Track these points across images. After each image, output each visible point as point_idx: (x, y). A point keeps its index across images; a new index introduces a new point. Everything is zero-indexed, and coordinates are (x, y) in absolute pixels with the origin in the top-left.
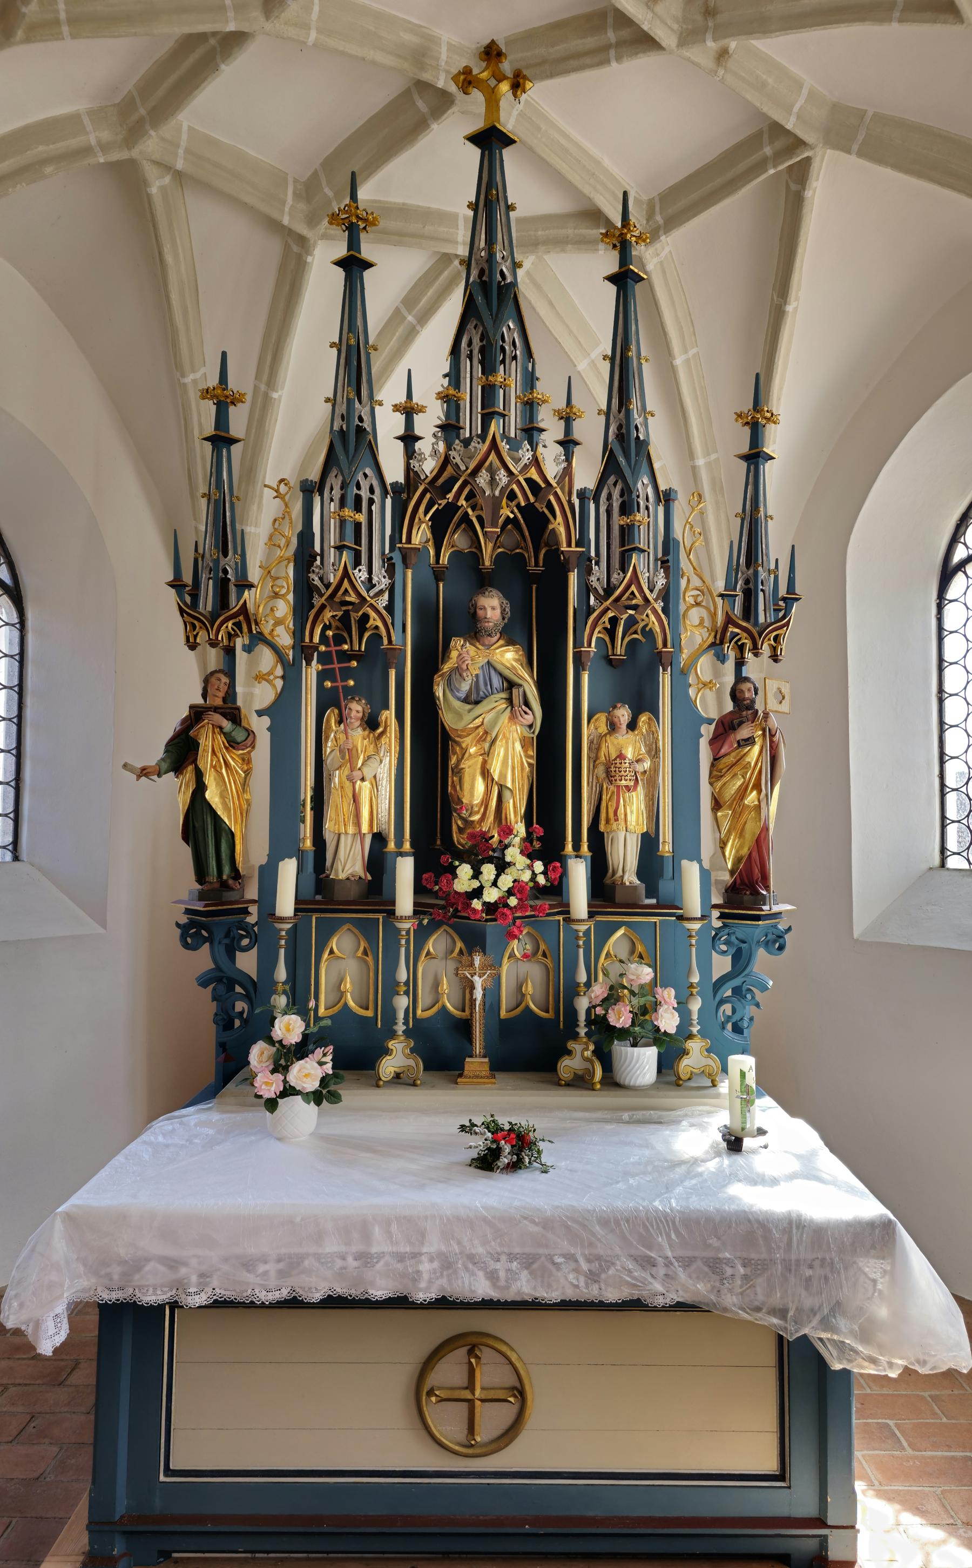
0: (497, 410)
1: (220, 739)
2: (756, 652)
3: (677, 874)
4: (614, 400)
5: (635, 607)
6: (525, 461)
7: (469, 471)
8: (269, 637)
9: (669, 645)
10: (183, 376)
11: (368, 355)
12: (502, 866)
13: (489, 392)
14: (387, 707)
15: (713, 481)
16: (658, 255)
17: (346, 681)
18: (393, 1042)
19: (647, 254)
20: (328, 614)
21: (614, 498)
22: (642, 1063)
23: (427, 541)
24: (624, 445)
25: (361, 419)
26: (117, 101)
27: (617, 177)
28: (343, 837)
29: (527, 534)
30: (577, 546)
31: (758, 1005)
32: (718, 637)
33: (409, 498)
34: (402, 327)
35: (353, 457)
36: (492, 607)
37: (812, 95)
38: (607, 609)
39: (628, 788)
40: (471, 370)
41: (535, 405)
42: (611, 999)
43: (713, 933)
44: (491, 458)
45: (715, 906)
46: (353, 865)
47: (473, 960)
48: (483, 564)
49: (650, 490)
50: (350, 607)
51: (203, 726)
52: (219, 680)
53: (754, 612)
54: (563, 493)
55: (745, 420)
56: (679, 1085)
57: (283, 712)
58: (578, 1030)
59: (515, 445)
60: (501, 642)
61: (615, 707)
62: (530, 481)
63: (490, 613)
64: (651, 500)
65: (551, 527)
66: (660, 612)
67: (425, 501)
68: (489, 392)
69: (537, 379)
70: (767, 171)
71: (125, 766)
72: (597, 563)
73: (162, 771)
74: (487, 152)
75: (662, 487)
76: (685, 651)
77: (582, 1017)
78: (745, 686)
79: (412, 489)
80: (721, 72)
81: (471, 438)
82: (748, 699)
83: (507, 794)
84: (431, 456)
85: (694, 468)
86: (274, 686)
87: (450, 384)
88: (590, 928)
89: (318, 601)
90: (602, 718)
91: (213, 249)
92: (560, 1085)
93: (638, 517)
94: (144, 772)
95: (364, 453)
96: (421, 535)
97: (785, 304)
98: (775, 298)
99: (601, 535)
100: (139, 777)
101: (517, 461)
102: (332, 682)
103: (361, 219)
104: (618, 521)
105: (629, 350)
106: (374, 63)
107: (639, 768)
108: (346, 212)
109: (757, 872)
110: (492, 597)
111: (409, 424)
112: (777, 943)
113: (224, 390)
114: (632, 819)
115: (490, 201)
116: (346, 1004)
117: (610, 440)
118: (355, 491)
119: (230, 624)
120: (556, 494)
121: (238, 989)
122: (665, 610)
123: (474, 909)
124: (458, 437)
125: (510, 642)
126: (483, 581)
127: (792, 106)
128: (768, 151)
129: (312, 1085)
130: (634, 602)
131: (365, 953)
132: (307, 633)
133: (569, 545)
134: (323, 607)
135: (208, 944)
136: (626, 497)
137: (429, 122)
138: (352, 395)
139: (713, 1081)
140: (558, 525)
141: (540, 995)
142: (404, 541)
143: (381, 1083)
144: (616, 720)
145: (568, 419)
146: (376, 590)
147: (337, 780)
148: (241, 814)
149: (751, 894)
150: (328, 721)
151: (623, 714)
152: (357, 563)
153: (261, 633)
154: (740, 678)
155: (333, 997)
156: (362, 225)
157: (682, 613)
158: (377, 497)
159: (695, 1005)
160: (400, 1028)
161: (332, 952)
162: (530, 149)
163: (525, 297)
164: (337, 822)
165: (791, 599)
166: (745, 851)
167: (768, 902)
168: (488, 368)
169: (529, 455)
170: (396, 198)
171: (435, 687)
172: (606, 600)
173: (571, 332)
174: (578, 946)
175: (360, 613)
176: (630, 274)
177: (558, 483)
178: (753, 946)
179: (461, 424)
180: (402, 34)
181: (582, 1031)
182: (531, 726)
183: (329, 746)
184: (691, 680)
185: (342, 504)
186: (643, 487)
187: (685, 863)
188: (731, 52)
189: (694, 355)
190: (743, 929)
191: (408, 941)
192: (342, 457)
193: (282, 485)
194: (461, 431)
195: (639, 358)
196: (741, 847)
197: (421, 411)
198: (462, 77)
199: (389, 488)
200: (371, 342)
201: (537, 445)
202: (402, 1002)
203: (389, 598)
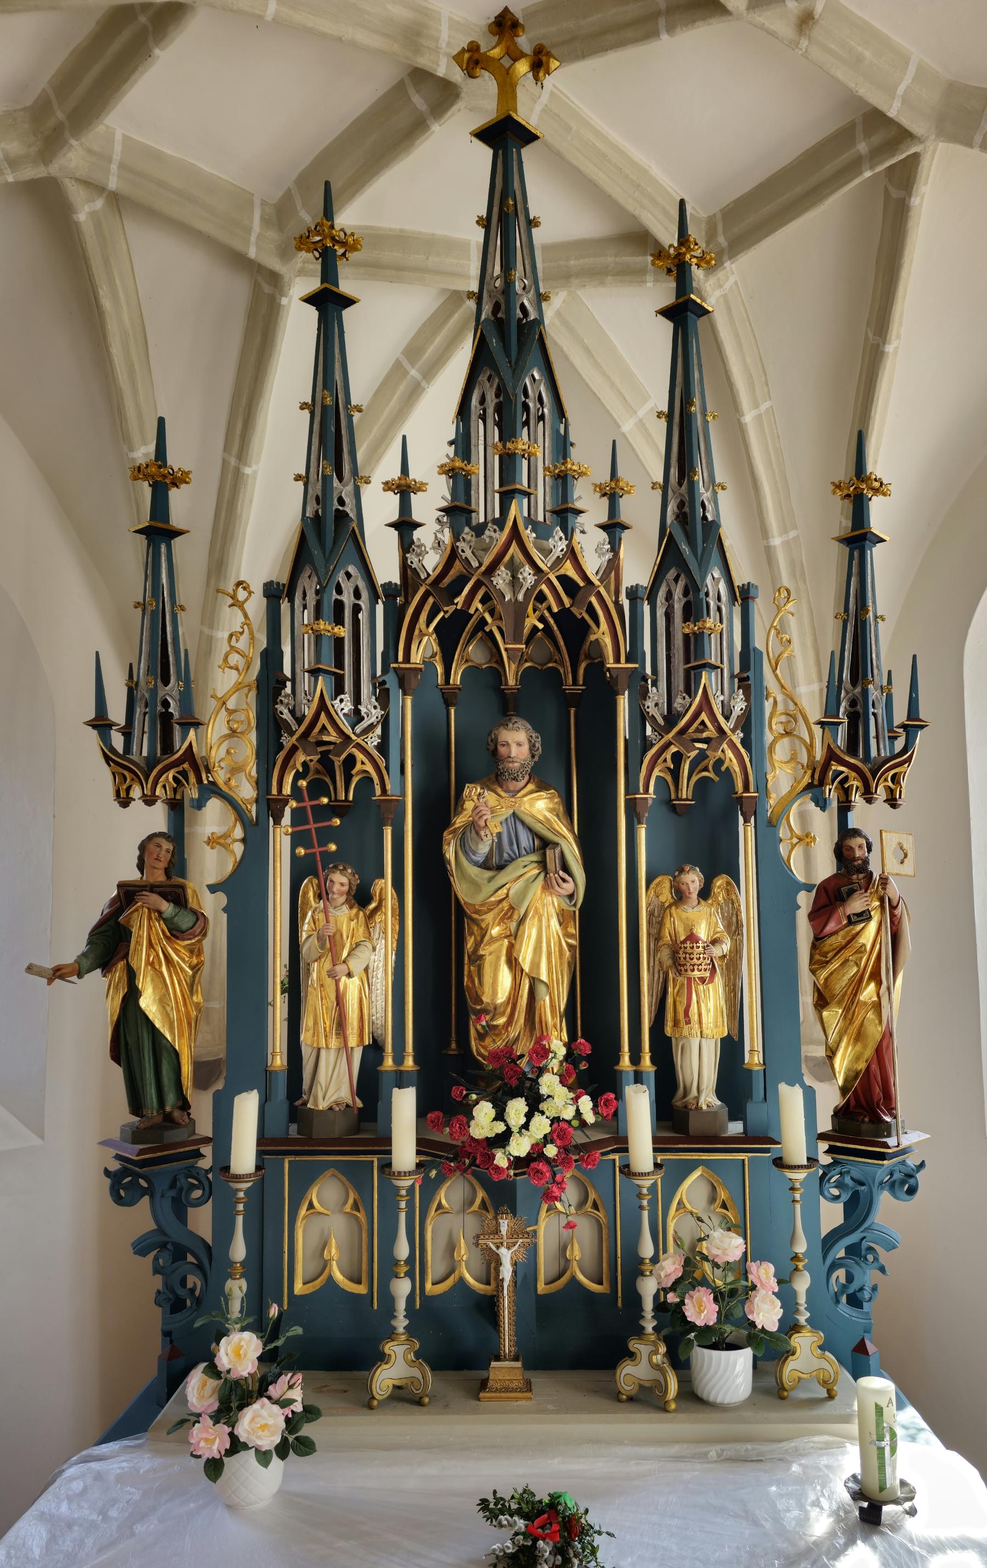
0: (518, 486)
1: (159, 927)
2: (868, 796)
3: (769, 1096)
4: (672, 470)
5: (707, 741)
6: (557, 553)
7: (483, 568)
8: (224, 788)
9: (752, 789)
10: (131, 449)
11: (350, 417)
12: (535, 1103)
13: (508, 462)
14: (382, 875)
15: (792, 564)
16: (721, 286)
17: (326, 845)
18: (391, 1344)
19: (708, 284)
20: (301, 757)
21: (676, 598)
22: (730, 1373)
23: (434, 655)
24: (688, 528)
25: (341, 502)
26: (29, 102)
27: (669, 189)
28: (323, 1053)
29: (562, 643)
30: (627, 661)
31: (882, 1269)
32: (816, 776)
33: (407, 603)
34: (404, 384)
35: (331, 552)
36: (518, 742)
37: (922, 71)
38: (669, 744)
39: (703, 980)
40: (484, 435)
41: (569, 478)
42: (689, 1279)
43: (821, 1172)
44: (511, 551)
45: (822, 1137)
46: (338, 1089)
47: (498, 1225)
48: (506, 684)
49: (722, 587)
50: (331, 747)
51: (137, 910)
52: (159, 846)
53: (864, 744)
54: (608, 592)
55: (846, 492)
56: (783, 1398)
57: (244, 887)
58: (643, 1323)
59: (542, 532)
60: (531, 787)
61: (682, 871)
62: (564, 579)
63: (514, 751)
64: (724, 598)
65: (593, 638)
66: (739, 746)
67: (427, 608)
68: (508, 462)
69: (572, 445)
70: (861, 173)
71: (30, 969)
72: (655, 684)
73: (83, 971)
74: (500, 152)
75: (738, 582)
76: (773, 795)
77: (648, 1305)
78: (856, 842)
79: (410, 590)
80: (804, 43)
81: (485, 525)
82: (859, 858)
83: (541, 990)
84: (433, 548)
85: (769, 551)
86: (233, 852)
87: (456, 454)
88: (656, 1182)
89: (288, 741)
90: (664, 883)
91: (160, 288)
92: (620, 1401)
93: (710, 623)
94: (58, 973)
95: (346, 546)
96: (424, 648)
97: (884, 343)
98: (870, 335)
99: (659, 645)
100: (50, 981)
101: (546, 552)
102: (305, 849)
103: (338, 242)
104: (681, 628)
105: (691, 404)
106: (353, 44)
107: (717, 951)
108: (318, 234)
109: (877, 1090)
110: (518, 729)
111: (405, 506)
112: (906, 1184)
113: (160, 467)
114: (709, 1019)
115: (505, 215)
116: (330, 1278)
117: (669, 521)
118: (335, 596)
119: (171, 774)
120: (599, 596)
121: (190, 1258)
122: (746, 743)
123: (497, 1168)
124: (468, 523)
125: (542, 787)
126: (507, 706)
127: (896, 87)
128: (862, 147)
129: (270, 1441)
130: (705, 735)
131: (356, 1206)
132: (274, 783)
133: (617, 660)
134: (294, 749)
135: (146, 1198)
136: (691, 597)
137: (428, 122)
138: (328, 471)
139: (829, 1391)
140: (602, 634)
141: (590, 1264)
142: (400, 659)
143: (375, 1403)
144: (684, 887)
145: (612, 495)
146: (364, 724)
147: (315, 975)
148: (189, 1024)
149: (870, 1121)
150: (305, 893)
151: (693, 880)
152: (339, 690)
153: (214, 783)
154: (846, 832)
155: (313, 1268)
156: (340, 251)
157: (767, 746)
158: (364, 603)
159: (802, 1284)
160: (401, 1323)
161: (311, 1206)
162: (559, 155)
163: (556, 343)
164: (315, 1033)
165: (913, 727)
166: (862, 1066)
167: (894, 1132)
168: (507, 433)
169: (563, 545)
170: (389, 222)
171: (445, 847)
172: (668, 733)
173: (613, 385)
174: (641, 1208)
175: (344, 756)
176: (690, 306)
177: (601, 580)
178: (875, 1190)
179: (473, 506)
180: (389, 6)
181: (649, 1325)
182: (571, 897)
183: (305, 929)
184: (783, 832)
185: (318, 615)
186: (714, 583)
187: (783, 1088)
188: (816, 17)
189: (767, 410)
190: (858, 1167)
191: (410, 1205)
192: (316, 552)
193: (240, 589)
194: (474, 515)
195: (704, 415)
196: (857, 1058)
197: (420, 489)
198: (467, 56)
199: (380, 590)
200: (354, 402)
201: (573, 530)
202: (402, 1288)
203: (381, 733)
